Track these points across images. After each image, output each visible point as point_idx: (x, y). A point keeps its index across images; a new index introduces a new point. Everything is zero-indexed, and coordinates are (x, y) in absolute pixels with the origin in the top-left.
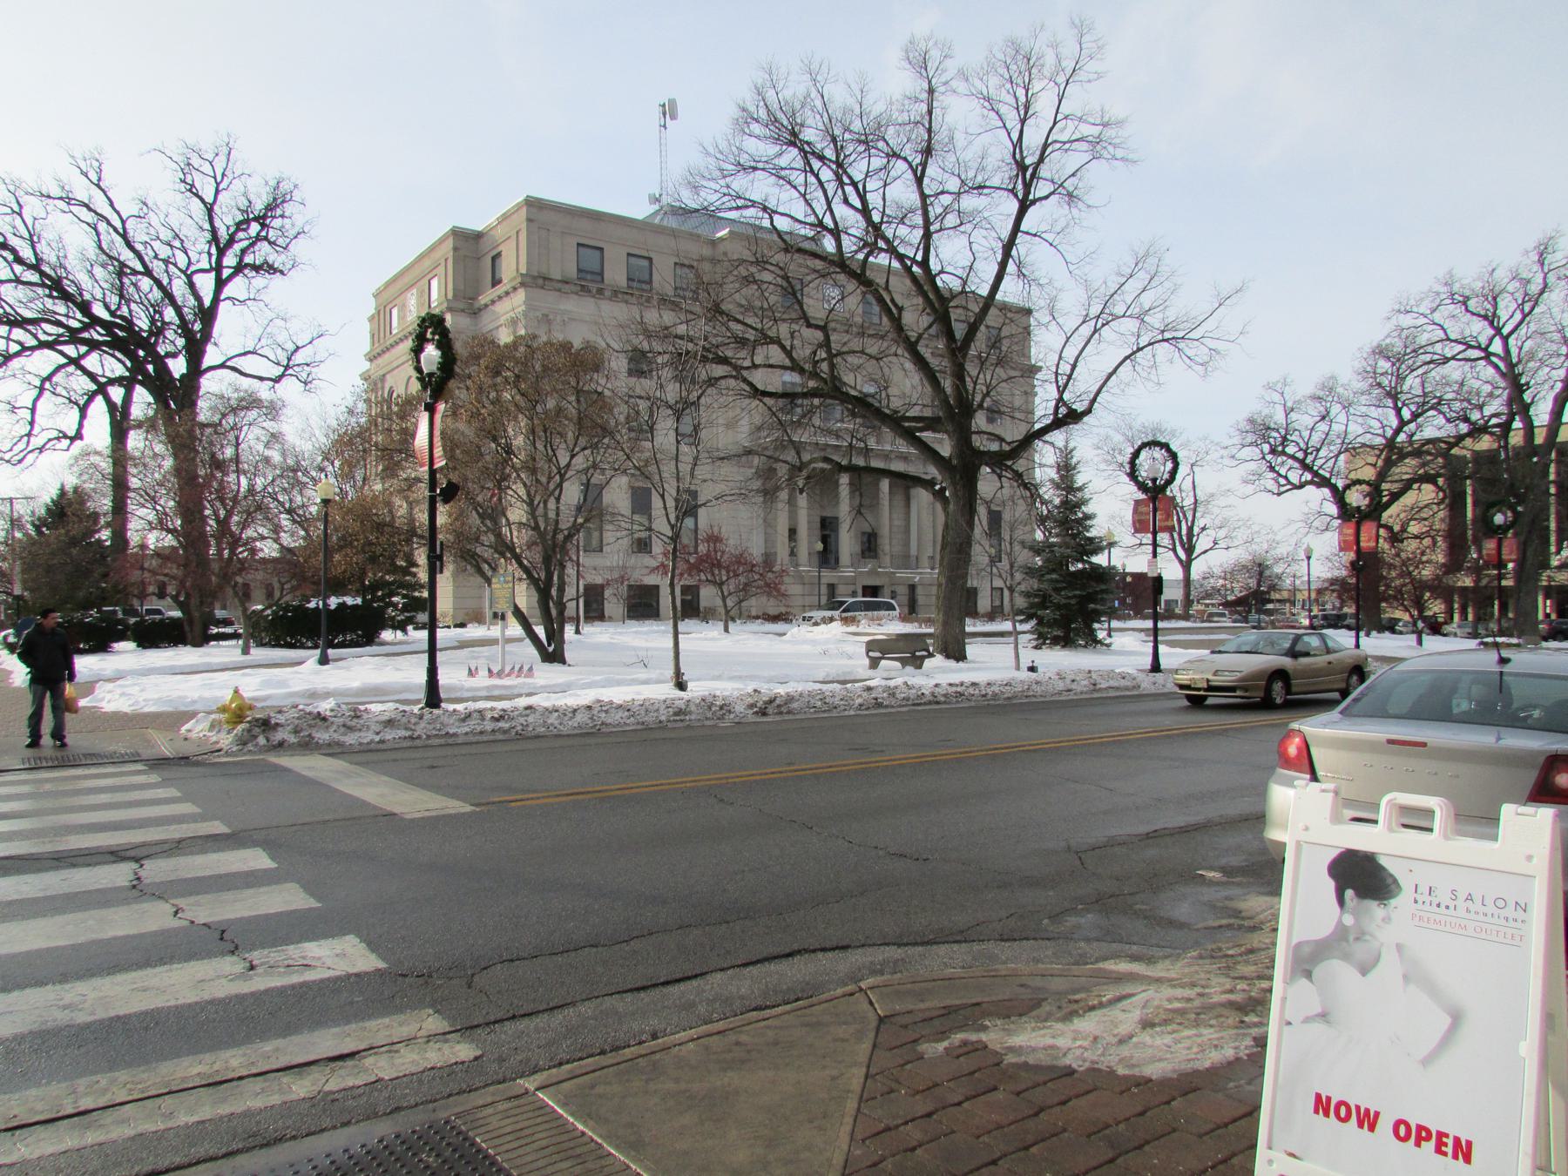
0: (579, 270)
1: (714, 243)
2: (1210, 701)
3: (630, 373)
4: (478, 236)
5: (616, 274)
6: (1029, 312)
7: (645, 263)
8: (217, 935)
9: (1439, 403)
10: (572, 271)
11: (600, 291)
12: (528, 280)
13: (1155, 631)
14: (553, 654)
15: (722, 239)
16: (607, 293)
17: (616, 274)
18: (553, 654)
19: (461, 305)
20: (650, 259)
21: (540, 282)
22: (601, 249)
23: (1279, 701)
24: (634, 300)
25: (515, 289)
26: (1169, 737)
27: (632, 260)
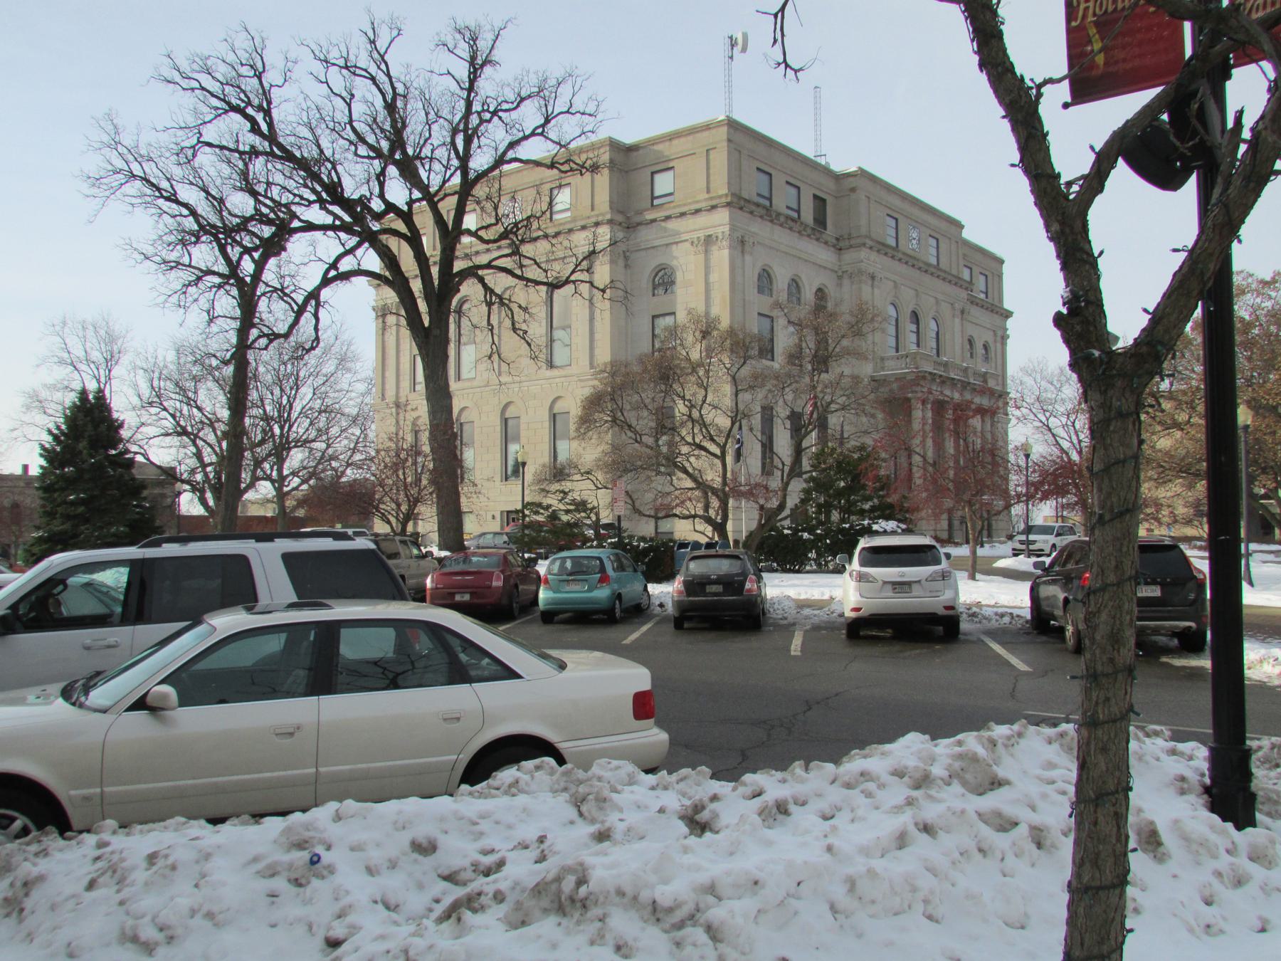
19: (620, 218)
21: (742, 203)
25: (714, 207)
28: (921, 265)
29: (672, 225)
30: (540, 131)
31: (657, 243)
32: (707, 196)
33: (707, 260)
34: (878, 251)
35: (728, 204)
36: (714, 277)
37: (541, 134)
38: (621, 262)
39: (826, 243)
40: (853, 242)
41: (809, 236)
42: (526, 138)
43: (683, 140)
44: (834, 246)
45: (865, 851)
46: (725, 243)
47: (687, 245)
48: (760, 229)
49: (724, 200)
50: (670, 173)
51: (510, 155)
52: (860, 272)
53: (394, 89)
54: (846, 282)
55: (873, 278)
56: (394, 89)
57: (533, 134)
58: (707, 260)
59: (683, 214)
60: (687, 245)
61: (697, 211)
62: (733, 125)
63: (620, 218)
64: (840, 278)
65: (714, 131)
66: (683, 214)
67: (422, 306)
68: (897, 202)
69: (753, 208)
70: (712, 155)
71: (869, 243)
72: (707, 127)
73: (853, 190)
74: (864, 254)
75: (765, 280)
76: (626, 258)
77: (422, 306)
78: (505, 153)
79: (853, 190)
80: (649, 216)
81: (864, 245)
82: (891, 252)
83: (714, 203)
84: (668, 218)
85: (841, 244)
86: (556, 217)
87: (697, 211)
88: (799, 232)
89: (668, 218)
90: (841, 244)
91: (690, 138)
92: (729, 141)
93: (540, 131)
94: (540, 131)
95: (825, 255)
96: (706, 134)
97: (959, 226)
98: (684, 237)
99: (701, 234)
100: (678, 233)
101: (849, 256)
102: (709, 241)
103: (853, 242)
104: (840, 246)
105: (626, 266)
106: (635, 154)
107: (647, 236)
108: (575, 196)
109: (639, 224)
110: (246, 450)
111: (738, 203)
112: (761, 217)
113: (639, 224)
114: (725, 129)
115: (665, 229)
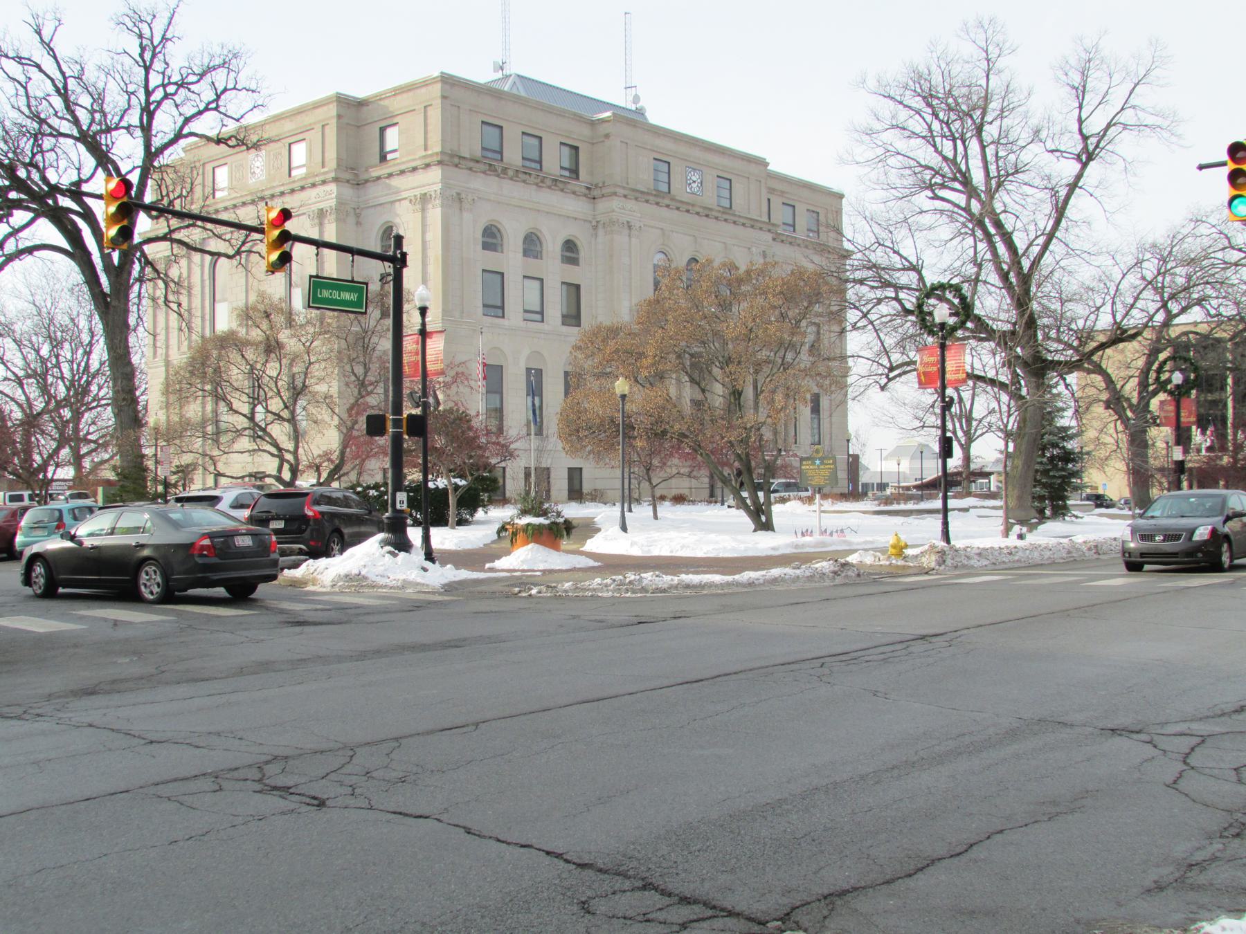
0: (483, 148)
1: (593, 124)
2: (1147, 567)
3: (655, 266)
4: (361, 104)
5: (555, 160)
6: (841, 196)
7: (535, 142)
8: (358, 791)
9: (1159, 291)
10: (478, 153)
11: (505, 170)
12: (446, 158)
13: (945, 510)
14: (767, 526)
15: (603, 121)
16: (510, 173)
17: (513, 155)
18: (767, 526)
19: (347, 176)
20: (540, 138)
21: (456, 160)
22: (501, 128)
23: (1226, 566)
24: (532, 180)
25: (428, 166)
26: (1117, 601)
27: (486, 128)
28: (698, 209)
29: (396, 182)
30: (214, 105)
31: (382, 200)
32: (424, 153)
33: (424, 218)
34: (636, 199)
35: (440, 163)
36: (429, 236)
37: (216, 109)
38: (351, 220)
39: (574, 193)
40: (604, 191)
41: (549, 187)
42: (200, 113)
43: (405, 96)
44: (585, 195)
45: (25, 509)
46: (438, 202)
47: (407, 202)
48: (482, 184)
49: (435, 159)
50: (396, 129)
51: (185, 131)
52: (612, 223)
53: (63, 74)
54: (601, 232)
55: (630, 227)
56: (63, 74)
57: (207, 109)
58: (424, 218)
59: (402, 172)
60: (407, 202)
61: (414, 169)
62: (448, 81)
63: (347, 176)
64: (595, 228)
65: (430, 88)
66: (402, 172)
67: (104, 280)
68: (668, 145)
69: (471, 164)
70: (430, 112)
71: (621, 191)
72: (425, 83)
73: (607, 136)
74: (615, 203)
75: (492, 238)
76: (358, 216)
77: (104, 280)
78: (182, 128)
79: (607, 136)
80: (375, 173)
81: (615, 194)
82: (983, 148)
83: (427, 161)
84: (390, 175)
85: (596, 193)
86: (294, 173)
87: (414, 169)
88: (537, 184)
89: (390, 175)
90: (596, 193)
91: (411, 94)
92: (444, 97)
93: (213, 106)
94: (213, 106)
95: (573, 206)
96: (423, 90)
97: (762, 163)
98: (404, 195)
99: (418, 192)
100: (398, 192)
101: (602, 205)
102: (424, 199)
103: (604, 191)
104: (592, 194)
105: (358, 223)
106: (365, 109)
107: (375, 193)
108: (310, 152)
109: (367, 181)
110: (108, 483)
111: (451, 160)
112: (484, 172)
113: (367, 181)
114: (439, 86)
115: (389, 187)
